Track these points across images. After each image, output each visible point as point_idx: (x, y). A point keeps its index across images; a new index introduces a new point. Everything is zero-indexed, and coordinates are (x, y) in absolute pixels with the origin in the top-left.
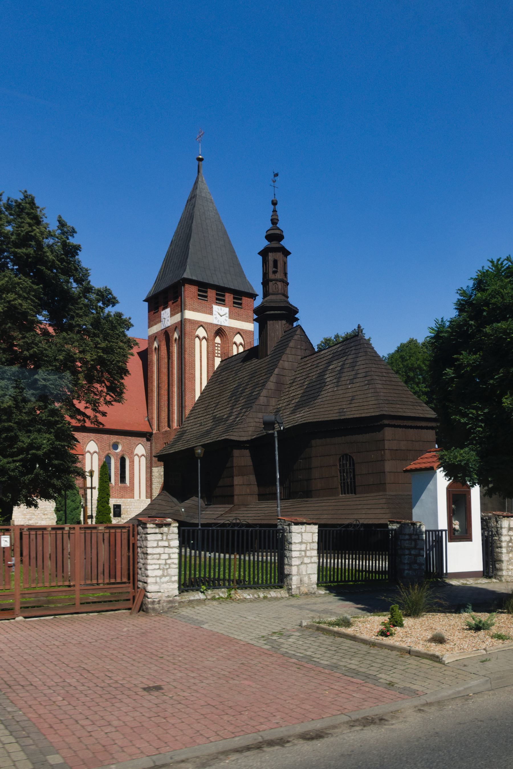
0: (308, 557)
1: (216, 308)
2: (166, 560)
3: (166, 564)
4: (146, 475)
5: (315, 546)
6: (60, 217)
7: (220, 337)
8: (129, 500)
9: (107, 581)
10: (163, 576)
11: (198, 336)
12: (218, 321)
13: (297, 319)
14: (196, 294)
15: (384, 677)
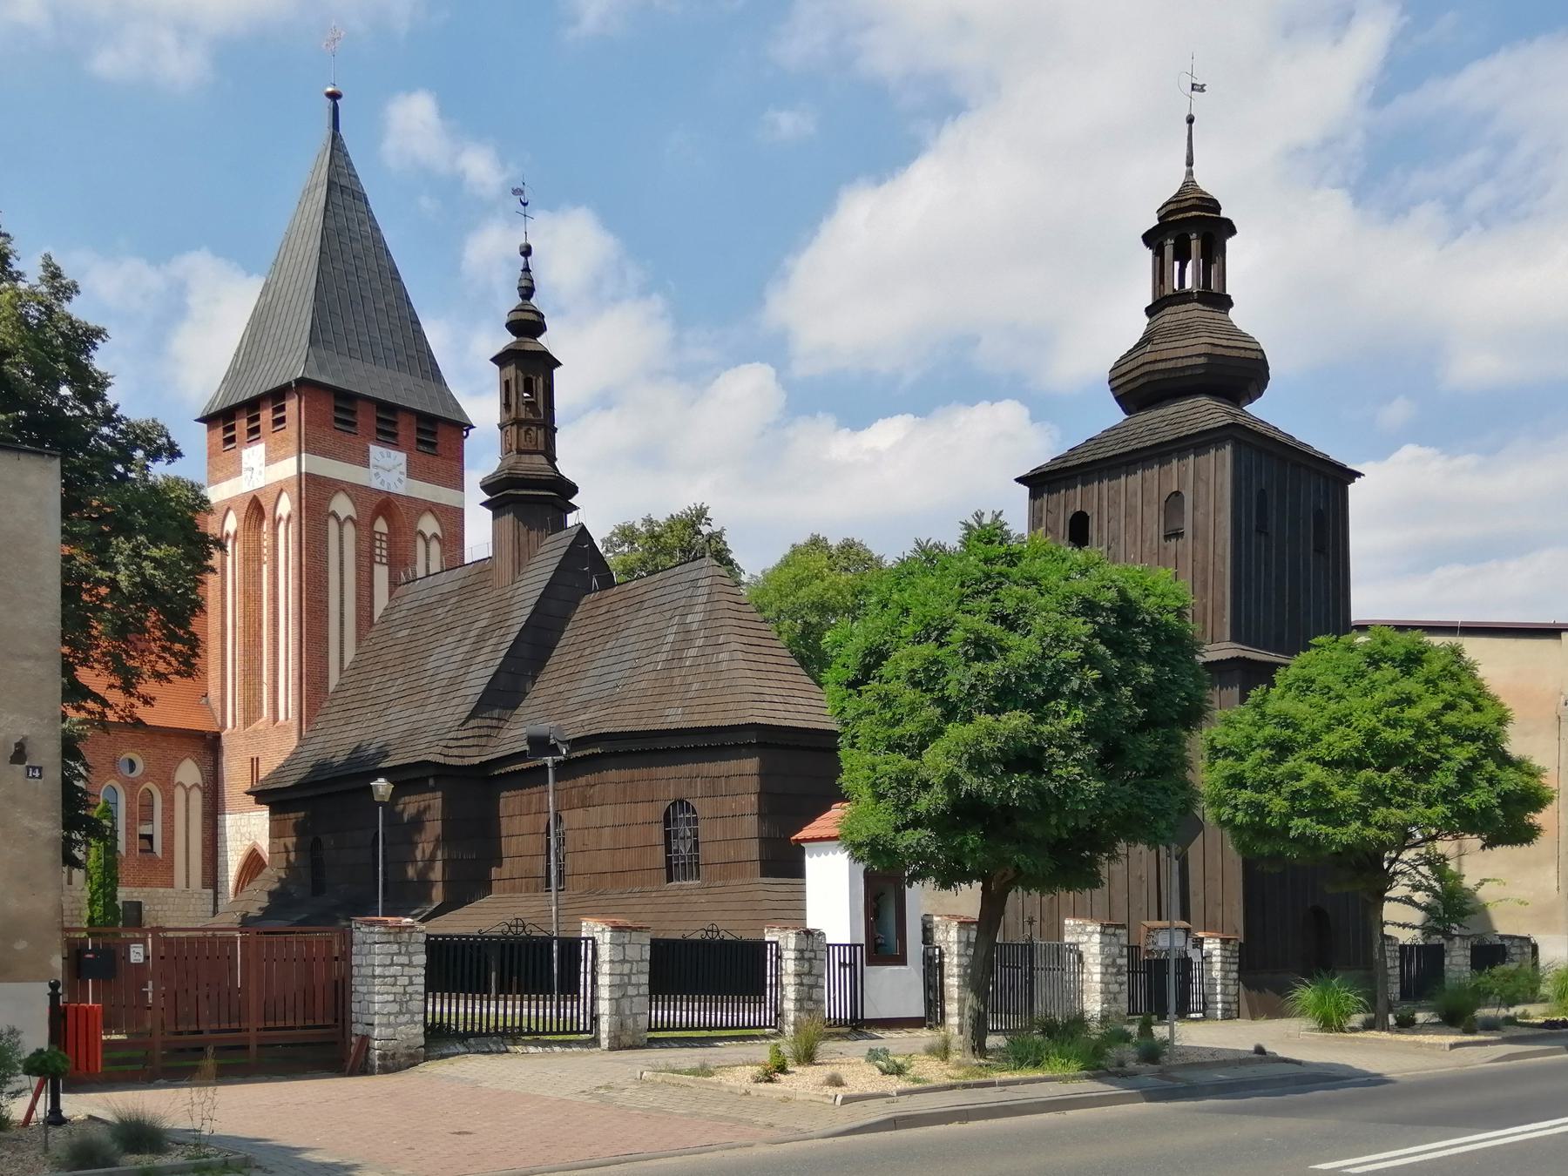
1: (376, 451)
3: (405, 993)
4: (204, 831)
5: (646, 967)
6: (48, 257)
7: (386, 520)
10: (401, 1013)
11: (334, 514)
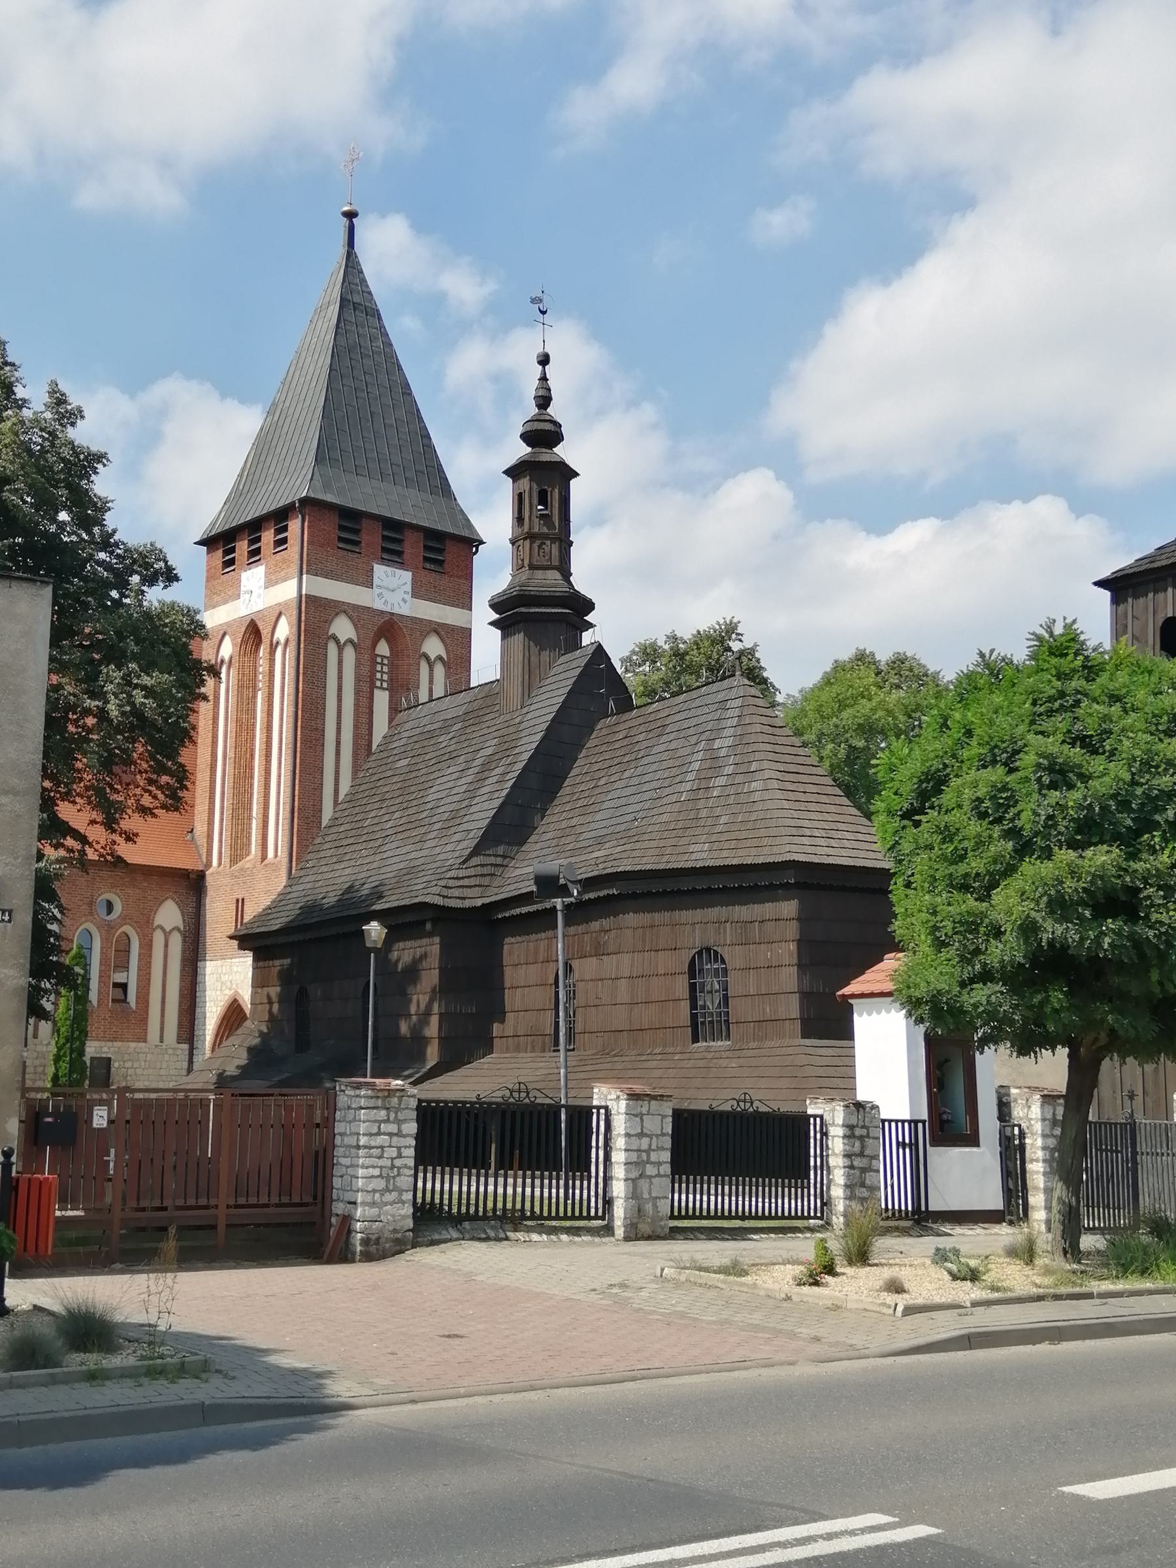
0: (652, 1163)
1: (381, 572)
2: (393, 1159)
3: (393, 1167)
8: (133, 1045)
9: (275, 1200)
10: (387, 1190)
11: (335, 638)
12: (386, 602)
13: (590, 625)
14: (334, 537)
15: (805, 1331)
